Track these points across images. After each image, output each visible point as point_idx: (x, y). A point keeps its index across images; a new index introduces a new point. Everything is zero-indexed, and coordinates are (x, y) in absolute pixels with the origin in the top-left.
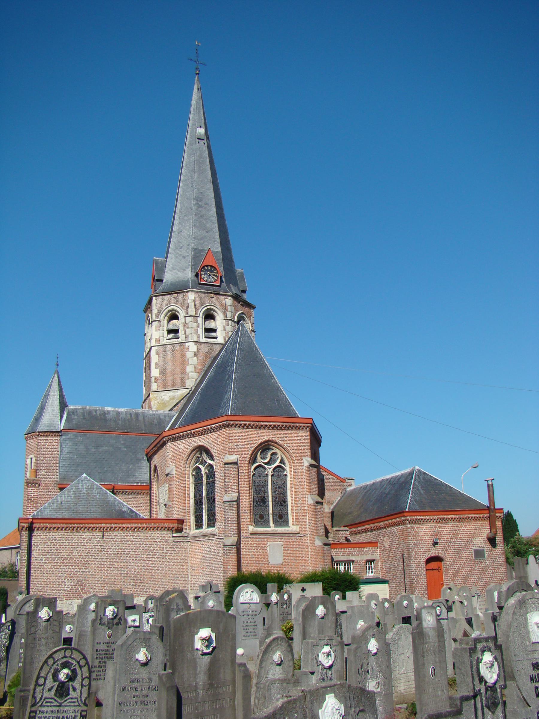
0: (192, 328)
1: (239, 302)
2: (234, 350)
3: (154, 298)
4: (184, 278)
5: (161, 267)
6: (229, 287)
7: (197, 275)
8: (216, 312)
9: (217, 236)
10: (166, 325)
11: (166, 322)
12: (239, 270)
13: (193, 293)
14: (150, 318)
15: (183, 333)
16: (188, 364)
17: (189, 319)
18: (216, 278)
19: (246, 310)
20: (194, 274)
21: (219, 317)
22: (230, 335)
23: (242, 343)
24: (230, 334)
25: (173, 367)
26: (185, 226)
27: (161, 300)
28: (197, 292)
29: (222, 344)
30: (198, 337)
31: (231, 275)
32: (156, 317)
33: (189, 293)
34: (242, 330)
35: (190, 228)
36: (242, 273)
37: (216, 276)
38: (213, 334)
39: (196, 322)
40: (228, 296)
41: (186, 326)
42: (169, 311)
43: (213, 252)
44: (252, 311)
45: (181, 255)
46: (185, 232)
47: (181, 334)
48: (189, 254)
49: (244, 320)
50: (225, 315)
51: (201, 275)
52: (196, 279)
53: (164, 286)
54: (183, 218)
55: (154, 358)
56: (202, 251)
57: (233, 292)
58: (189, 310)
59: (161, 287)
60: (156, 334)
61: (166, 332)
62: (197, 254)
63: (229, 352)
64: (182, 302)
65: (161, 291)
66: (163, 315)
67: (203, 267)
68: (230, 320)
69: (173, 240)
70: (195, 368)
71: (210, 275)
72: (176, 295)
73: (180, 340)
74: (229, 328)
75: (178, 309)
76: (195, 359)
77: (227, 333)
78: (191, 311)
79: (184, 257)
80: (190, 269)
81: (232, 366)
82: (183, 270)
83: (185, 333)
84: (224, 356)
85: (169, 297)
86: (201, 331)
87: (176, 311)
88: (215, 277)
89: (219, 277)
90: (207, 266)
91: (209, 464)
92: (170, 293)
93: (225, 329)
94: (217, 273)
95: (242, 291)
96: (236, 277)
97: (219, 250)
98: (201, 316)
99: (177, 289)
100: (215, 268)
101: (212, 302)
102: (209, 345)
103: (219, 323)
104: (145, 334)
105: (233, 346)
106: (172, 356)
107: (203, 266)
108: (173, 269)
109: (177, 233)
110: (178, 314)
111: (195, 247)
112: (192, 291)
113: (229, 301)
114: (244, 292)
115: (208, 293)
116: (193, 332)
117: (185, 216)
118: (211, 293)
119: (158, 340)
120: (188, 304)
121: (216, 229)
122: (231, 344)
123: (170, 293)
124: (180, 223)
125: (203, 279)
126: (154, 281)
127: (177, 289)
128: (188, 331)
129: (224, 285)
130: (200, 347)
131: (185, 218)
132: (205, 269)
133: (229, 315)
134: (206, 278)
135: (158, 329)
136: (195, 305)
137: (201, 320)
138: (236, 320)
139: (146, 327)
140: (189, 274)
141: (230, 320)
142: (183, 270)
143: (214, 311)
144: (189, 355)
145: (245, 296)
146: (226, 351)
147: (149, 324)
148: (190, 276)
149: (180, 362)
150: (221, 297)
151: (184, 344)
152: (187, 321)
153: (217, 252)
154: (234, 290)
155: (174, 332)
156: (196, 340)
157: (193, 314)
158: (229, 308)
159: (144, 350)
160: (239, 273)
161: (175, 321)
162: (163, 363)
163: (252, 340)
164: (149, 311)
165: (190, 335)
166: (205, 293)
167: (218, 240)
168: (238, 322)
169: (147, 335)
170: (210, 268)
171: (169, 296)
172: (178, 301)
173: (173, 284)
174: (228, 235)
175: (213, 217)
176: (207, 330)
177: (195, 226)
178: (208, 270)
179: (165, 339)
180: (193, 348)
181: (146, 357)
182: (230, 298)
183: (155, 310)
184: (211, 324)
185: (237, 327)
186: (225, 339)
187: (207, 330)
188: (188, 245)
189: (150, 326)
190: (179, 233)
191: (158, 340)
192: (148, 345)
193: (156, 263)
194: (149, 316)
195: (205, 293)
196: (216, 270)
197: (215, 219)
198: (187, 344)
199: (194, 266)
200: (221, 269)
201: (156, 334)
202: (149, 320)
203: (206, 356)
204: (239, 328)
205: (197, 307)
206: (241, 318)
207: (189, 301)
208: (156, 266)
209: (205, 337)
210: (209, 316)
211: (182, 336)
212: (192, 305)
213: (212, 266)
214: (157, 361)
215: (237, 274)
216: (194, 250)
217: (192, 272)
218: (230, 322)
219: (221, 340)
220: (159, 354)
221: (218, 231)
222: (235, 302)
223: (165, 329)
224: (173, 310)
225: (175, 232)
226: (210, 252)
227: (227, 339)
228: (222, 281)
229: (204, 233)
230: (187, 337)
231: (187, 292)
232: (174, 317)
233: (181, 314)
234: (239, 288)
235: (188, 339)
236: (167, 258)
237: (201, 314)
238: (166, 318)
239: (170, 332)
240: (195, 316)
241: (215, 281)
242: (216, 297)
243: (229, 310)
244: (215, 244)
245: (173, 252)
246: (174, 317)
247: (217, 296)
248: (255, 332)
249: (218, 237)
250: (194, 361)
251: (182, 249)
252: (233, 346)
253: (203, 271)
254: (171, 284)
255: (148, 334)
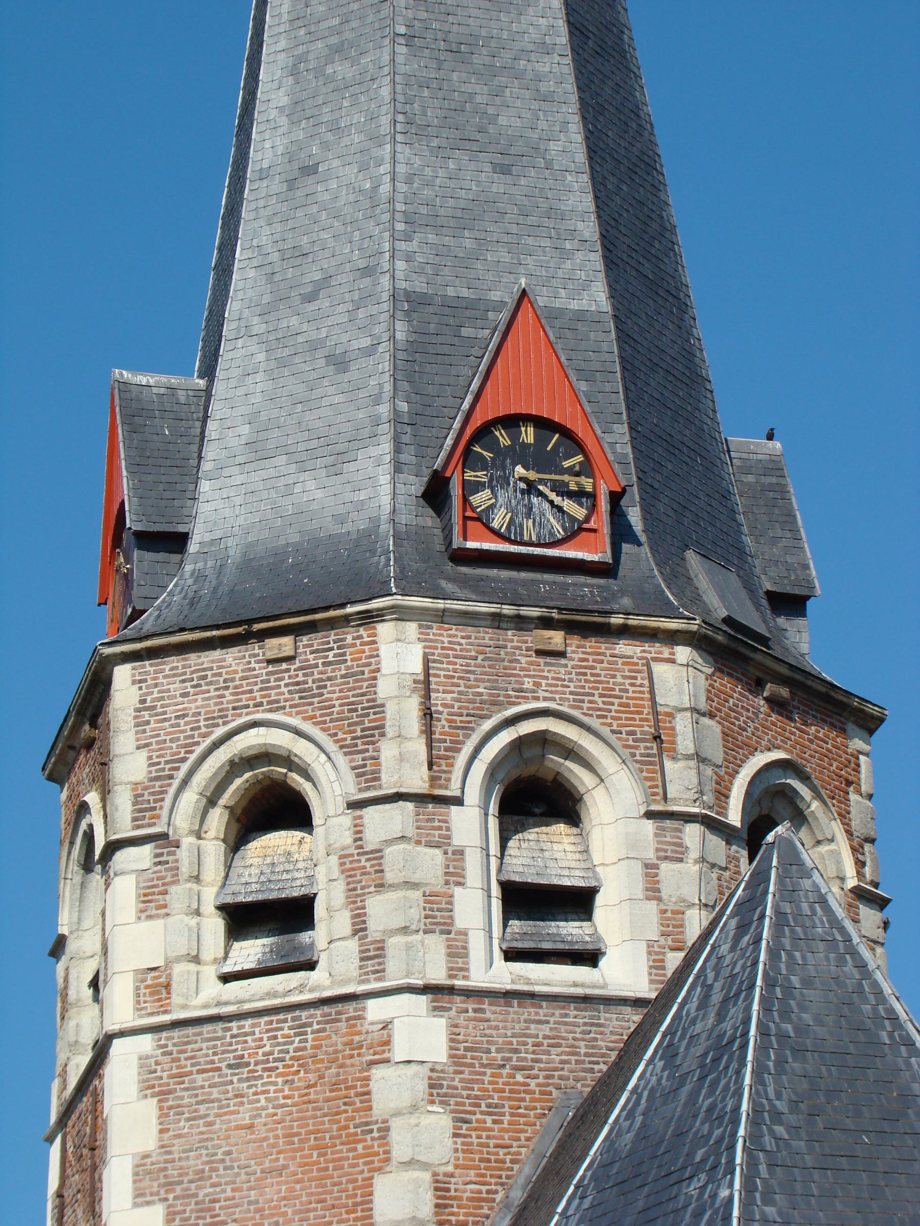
0: (404, 884)
1: (756, 686)
2: (727, 1048)
3: (122, 675)
4: (340, 519)
5: (166, 443)
6: (678, 577)
7: (435, 494)
8: (308, 777)
9: (578, 199)
10: (212, 871)
11: (213, 850)
12: (745, 442)
13: (412, 628)
14: (95, 818)
15: (343, 922)
16: (380, 1160)
17: (383, 822)
18: (577, 511)
19: (808, 740)
20: (417, 485)
21: (613, 800)
22: (693, 932)
23: (788, 990)
24: (695, 923)
25: (273, 1190)
26: (335, 128)
27: (176, 687)
28: (442, 617)
29: (637, 1003)
30: (458, 953)
31: (687, 485)
32: (144, 809)
33: (385, 630)
34: (788, 893)
35: (376, 139)
36: (774, 467)
37: (578, 495)
38: (571, 931)
39: (442, 842)
40: (673, 638)
41: (364, 869)
42: (236, 766)
43: (555, 314)
44: (857, 744)
45: (314, 346)
46: (341, 178)
47: (329, 930)
48: (373, 340)
49: (799, 818)
50: (657, 785)
51: (470, 488)
52: (429, 519)
53: (199, 577)
54: (319, 72)
55: (131, 1122)
56: (474, 309)
57: (706, 611)
58: (388, 751)
59: (173, 590)
60: (140, 937)
61: (215, 926)
62: (432, 332)
63: (689, 1062)
64: (333, 693)
65: (171, 618)
66: (190, 798)
67: (483, 433)
68: (688, 818)
69: (256, 234)
70: (441, 1188)
71: (531, 488)
72: (285, 644)
73: (318, 982)
74: (684, 880)
75: (302, 749)
76: (437, 1124)
77: (672, 922)
78: (403, 761)
79: (339, 363)
80: (385, 447)
81: (719, 1169)
82: (337, 455)
83: (359, 928)
84: (658, 1097)
85: (231, 659)
86: (475, 908)
87: (288, 761)
88: (568, 505)
89: (604, 504)
90: (512, 422)
91: (786, 486)
92: (241, 631)
93: (653, 891)
94: (587, 469)
95: (770, 595)
96: (726, 496)
97: (597, 298)
98: (473, 794)
99: (296, 604)
100: (567, 434)
101: (556, 686)
102: (545, 1009)
103: (607, 841)
104: (58, 947)
105: (721, 1016)
106: (264, 1103)
107: (477, 421)
108: (257, 451)
109: (277, 185)
110: (296, 780)
111: (419, 285)
112: (402, 614)
113: (679, 677)
114: (791, 604)
115: (520, 623)
116: (415, 914)
117: (338, 51)
118: (546, 623)
119: (156, 984)
120: (379, 708)
121: (569, 144)
122: (704, 1004)
123: (240, 630)
124: (296, 111)
125: (483, 519)
126: (117, 541)
127: (296, 604)
128: (382, 911)
129: (639, 558)
130: (471, 1032)
131: (341, 69)
132: (493, 446)
133: (682, 783)
134: (502, 509)
135: (152, 901)
136: (428, 715)
137: (471, 821)
138: (734, 817)
139: (68, 892)
140: (375, 490)
141: (688, 818)
142: (337, 455)
143: (571, 752)
144: (391, 1089)
145: (802, 640)
146: (669, 1053)
147: (87, 866)
148: (385, 500)
149: (321, 1149)
150: (624, 647)
151: (350, 1008)
152: (372, 839)
153: (580, 316)
154: (717, 596)
155: (280, 917)
156: (438, 975)
157: (417, 780)
158: (683, 725)
159: (47, 1066)
160: (747, 469)
161: (278, 842)
162: (194, 1163)
163: (862, 966)
164: (84, 768)
165: (395, 943)
166: (497, 621)
167: (589, 229)
168: (753, 835)
169: (72, 946)
170: (528, 435)
171: (231, 657)
172: (304, 693)
173: (260, 566)
174: (658, 188)
175: (546, 50)
176: (525, 900)
177: (412, 128)
178: (520, 454)
179: (210, 973)
180: (421, 1035)
181: (63, 1121)
182: (683, 653)
183: (130, 764)
184: (547, 856)
185: (746, 869)
186: (657, 965)
187: (525, 900)
188: (368, 271)
189: (96, 878)
190: (291, 184)
191: (156, 984)
192: (84, 1026)
193: (133, 410)
194: (84, 808)
195: (497, 621)
196: (580, 447)
197: (557, 70)
198: (375, 1010)
199: (410, 429)
200: (614, 442)
201: (140, 937)
202: (89, 837)
203: (516, 1093)
204: (759, 879)
205: (441, 727)
206: (773, 804)
207: (385, 689)
208: (133, 430)
209: (512, 955)
210: (535, 795)
211: (336, 959)
212: (404, 713)
213: (544, 425)
214: (149, 1141)
215: (739, 484)
216: (411, 303)
217: (398, 467)
218: (693, 831)
219: (626, 971)
220: (163, 1094)
221: (581, 157)
222: (724, 683)
223: (210, 897)
224: (265, 756)
225: (263, 175)
226: (526, 316)
227: (674, 960)
228: (621, 532)
229: (475, 177)
230: (373, 955)
231: (369, 618)
232: (274, 806)
233: (328, 785)
234: (749, 585)
235: (380, 973)
236: (209, 371)
237: (473, 781)
238: (217, 819)
239: (242, 919)
240: (434, 800)
241: (575, 531)
242: (578, 649)
243: (685, 742)
244: (565, 255)
245: (259, 327)
246: (274, 806)
247: (591, 644)
248: (881, 903)
249: (587, 202)
250: (425, 1137)
251: (323, 303)
252: (721, 1016)
253: (483, 464)
254: (249, 566)
255: (85, 944)
